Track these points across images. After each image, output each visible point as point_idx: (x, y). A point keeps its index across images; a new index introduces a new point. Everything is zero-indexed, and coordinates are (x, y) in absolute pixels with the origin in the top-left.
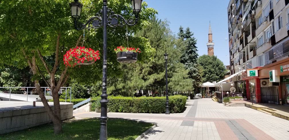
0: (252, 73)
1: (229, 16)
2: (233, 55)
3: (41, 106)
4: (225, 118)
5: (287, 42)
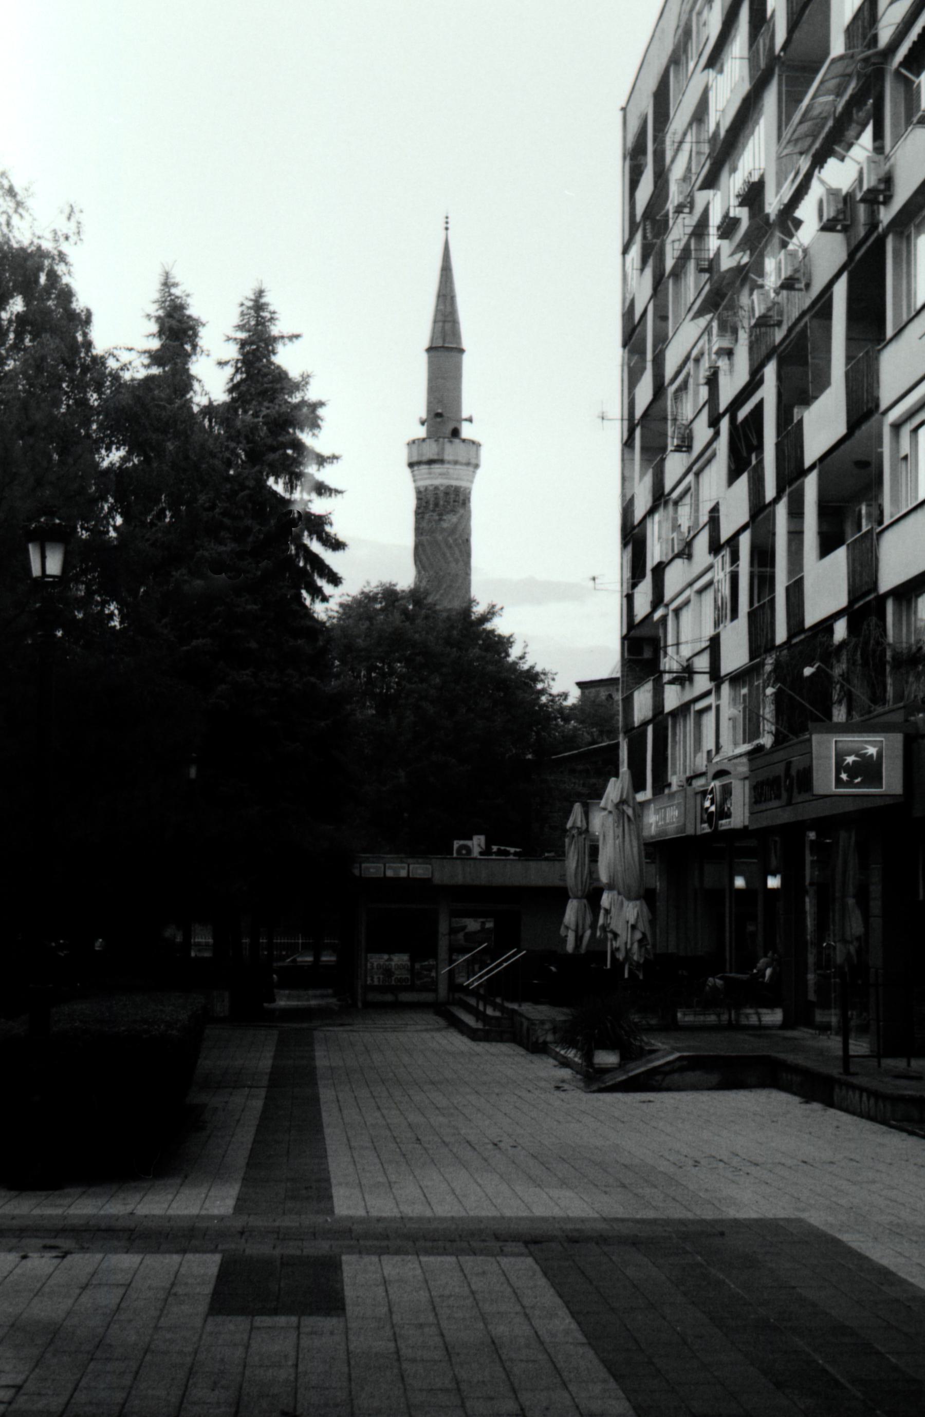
0: (850, 759)
1: (634, 184)
2: (660, 570)
3: (904, 413)
4: (557, 1212)
5: (625, 600)
